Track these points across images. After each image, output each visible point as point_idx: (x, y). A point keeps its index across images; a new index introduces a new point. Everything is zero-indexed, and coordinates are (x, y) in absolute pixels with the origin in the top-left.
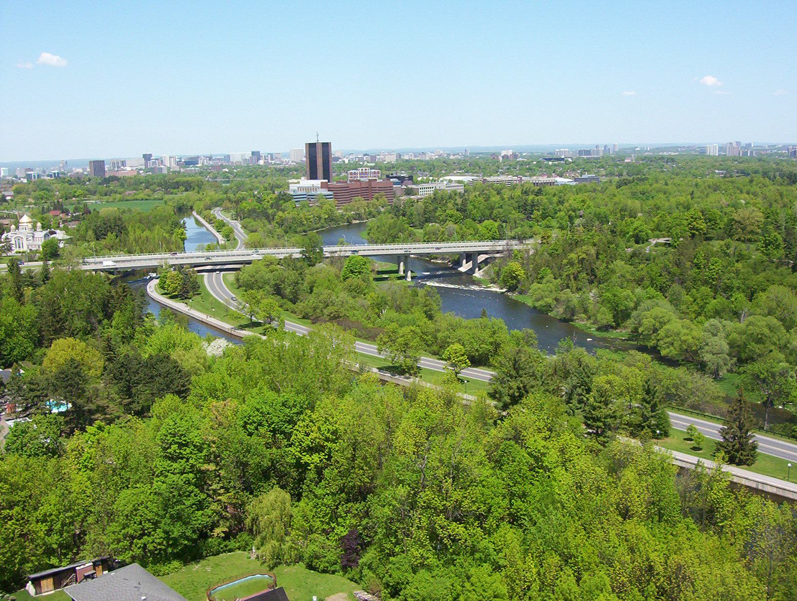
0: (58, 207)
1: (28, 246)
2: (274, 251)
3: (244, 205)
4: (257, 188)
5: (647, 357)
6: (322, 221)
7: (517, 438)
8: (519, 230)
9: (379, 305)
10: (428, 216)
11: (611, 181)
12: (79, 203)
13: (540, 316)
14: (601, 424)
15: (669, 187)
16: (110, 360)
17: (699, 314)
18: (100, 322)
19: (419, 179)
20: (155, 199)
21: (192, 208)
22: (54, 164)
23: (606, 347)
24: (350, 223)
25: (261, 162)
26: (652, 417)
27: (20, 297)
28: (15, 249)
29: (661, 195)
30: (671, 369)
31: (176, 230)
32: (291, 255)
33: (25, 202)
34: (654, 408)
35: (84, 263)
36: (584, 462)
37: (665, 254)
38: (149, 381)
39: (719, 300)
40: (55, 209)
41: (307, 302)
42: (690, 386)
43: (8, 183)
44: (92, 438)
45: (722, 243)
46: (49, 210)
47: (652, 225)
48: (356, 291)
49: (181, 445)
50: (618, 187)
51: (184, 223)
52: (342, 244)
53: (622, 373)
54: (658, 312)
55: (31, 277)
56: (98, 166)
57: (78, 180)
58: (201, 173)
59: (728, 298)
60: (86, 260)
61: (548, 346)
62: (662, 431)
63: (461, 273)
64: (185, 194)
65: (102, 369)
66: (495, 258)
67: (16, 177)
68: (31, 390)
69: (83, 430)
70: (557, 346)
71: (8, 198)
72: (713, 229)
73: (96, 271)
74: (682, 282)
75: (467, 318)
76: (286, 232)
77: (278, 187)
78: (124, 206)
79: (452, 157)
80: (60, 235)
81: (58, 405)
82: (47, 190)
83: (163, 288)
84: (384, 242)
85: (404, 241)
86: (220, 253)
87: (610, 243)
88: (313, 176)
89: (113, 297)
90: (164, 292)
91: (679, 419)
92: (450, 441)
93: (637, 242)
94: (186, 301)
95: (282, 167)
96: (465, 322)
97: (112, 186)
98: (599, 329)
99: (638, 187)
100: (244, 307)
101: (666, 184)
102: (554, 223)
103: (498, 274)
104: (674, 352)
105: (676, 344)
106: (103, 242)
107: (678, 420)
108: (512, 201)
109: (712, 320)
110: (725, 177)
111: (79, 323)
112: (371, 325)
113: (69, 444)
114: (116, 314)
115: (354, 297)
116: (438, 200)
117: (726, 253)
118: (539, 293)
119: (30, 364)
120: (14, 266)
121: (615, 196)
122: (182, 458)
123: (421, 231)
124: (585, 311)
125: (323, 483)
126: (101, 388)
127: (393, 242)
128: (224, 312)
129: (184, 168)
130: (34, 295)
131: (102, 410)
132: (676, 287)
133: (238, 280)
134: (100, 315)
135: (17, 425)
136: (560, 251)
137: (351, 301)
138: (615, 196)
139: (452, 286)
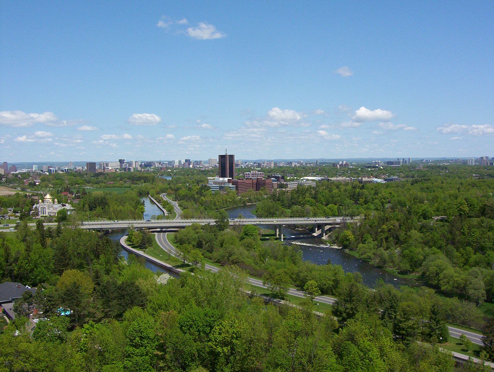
0: (68, 190)
1: (49, 213)
2: (198, 221)
3: (181, 192)
4: (188, 182)
5: (433, 291)
6: (228, 203)
7: (352, 338)
8: (350, 211)
9: (263, 256)
10: (296, 201)
11: (407, 181)
12: (79, 188)
13: (364, 264)
14: (404, 332)
15: (444, 185)
16: (98, 284)
17: (465, 264)
18: (92, 260)
19: (288, 178)
20: (126, 187)
21: (148, 193)
22: (67, 164)
23: (406, 284)
24: (245, 206)
25: (191, 166)
26: (437, 329)
27: (44, 245)
28: (41, 215)
29: (440, 190)
30: (448, 299)
31: (139, 206)
32: (209, 224)
33: (47, 186)
34: (438, 322)
35: (82, 225)
36: (395, 356)
37: (443, 226)
38: (123, 298)
39: (478, 255)
40: (65, 191)
41: (218, 253)
42: (460, 309)
43: (37, 175)
44: (87, 332)
45: (479, 219)
46: (61, 192)
47: (434, 208)
48: (249, 247)
49: (141, 338)
50: (412, 184)
51: (144, 202)
52: (240, 217)
53: (418, 300)
54: (439, 261)
55: (50, 232)
56: (91, 166)
57: (79, 174)
58: (154, 172)
59: (483, 254)
60: (84, 223)
61: (370, 283)
62: (444, 338)
63: (314, 237)
64: (144, 184)
65: (92, 290)
66: (336, 227)
67: (42, 171)
68: (50, 301)
69: (82, 327)
70: (374, 283)
71: (37, 184)
72: (473, 211)
73: (89, 229)
74: (453, 243)
75: (319, 264)
76: (206, 209)
77: (201, 181)
78: (107, 191)
79: (309, 165)
80: (68, 207)
81: (65, 311)
82: (60, 179)
83: (130, 241)
84: (267, 217)
85: (279, 216)
86: (166, 221)
87: (407, 219)
88: (223, 176)
89: (100, 245)
90: (130, 243)
91: (453, 330)
92: (310, 340)
93: (425, 219)
94: (144, 250)
95: (203, 169)
96: (317, 267)
97: (100, 178)
98: (399, 273)
99: (425, 185)
100: (180, 254)
101: (442, 183)
102: (372, 206)
103: (337, 238)
104: (450, 288)
105: (451, 283)
106: (94, 212)
107: (454, 331)
108: (347, 193)
109: (473, 268)
110: (479, 179)
111: (77, 261)
112: (258, 268)
113: (72, 335)
114: (102, 256)
115: (248, 250)
116: (301, 191)
117: (482, 226)
118: (368, 249)
119: (48, 285)
120: (40, 225)
121: (410, 190)
122: (142, 346)
123: (290, 210)
124: (392, 262)
125: (230, 365)
126: (91, 302)
127: (272, 217)
128: (168, 258)
129: (144, 168)
130: (52, 243)
131: (90, 315)
132: (450, 247)
133: (176, 238)
134: (92, 256)
135: (41, 321)
136: (376, 224)
137: (247, 252)
138: (410, 190)
139: (309, 245)
